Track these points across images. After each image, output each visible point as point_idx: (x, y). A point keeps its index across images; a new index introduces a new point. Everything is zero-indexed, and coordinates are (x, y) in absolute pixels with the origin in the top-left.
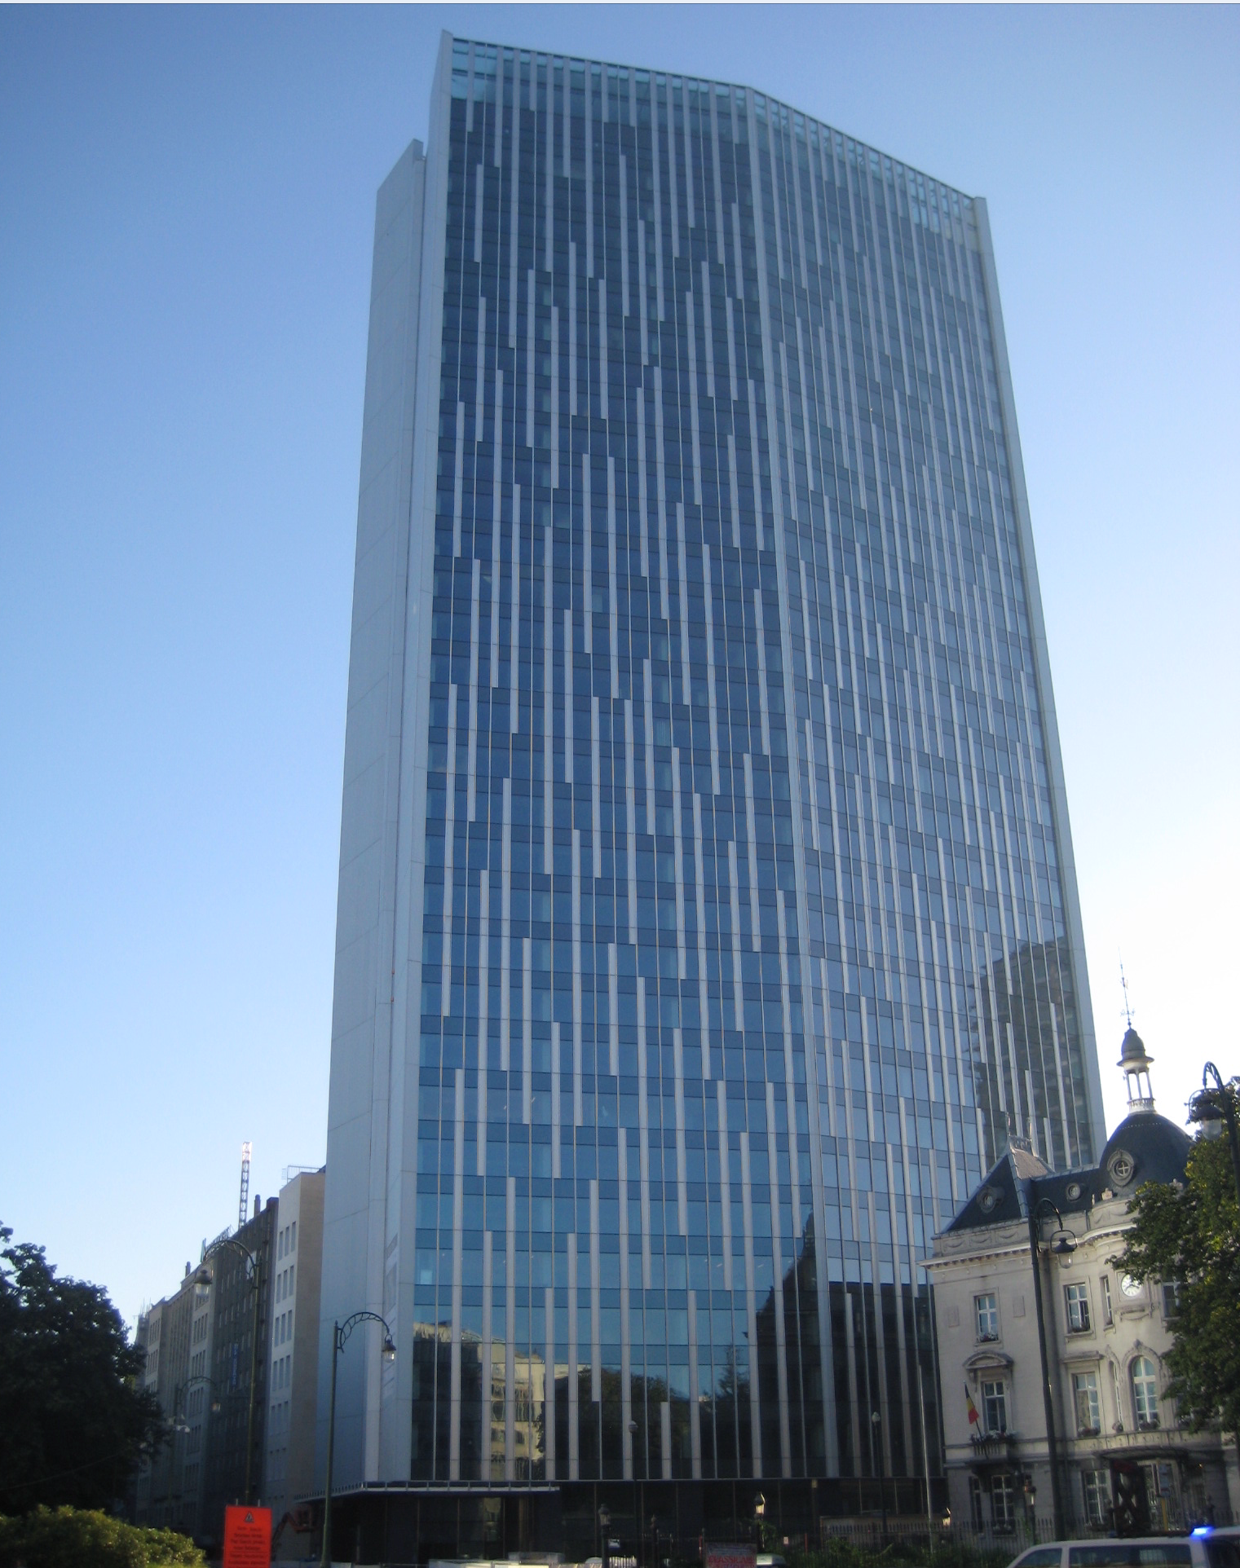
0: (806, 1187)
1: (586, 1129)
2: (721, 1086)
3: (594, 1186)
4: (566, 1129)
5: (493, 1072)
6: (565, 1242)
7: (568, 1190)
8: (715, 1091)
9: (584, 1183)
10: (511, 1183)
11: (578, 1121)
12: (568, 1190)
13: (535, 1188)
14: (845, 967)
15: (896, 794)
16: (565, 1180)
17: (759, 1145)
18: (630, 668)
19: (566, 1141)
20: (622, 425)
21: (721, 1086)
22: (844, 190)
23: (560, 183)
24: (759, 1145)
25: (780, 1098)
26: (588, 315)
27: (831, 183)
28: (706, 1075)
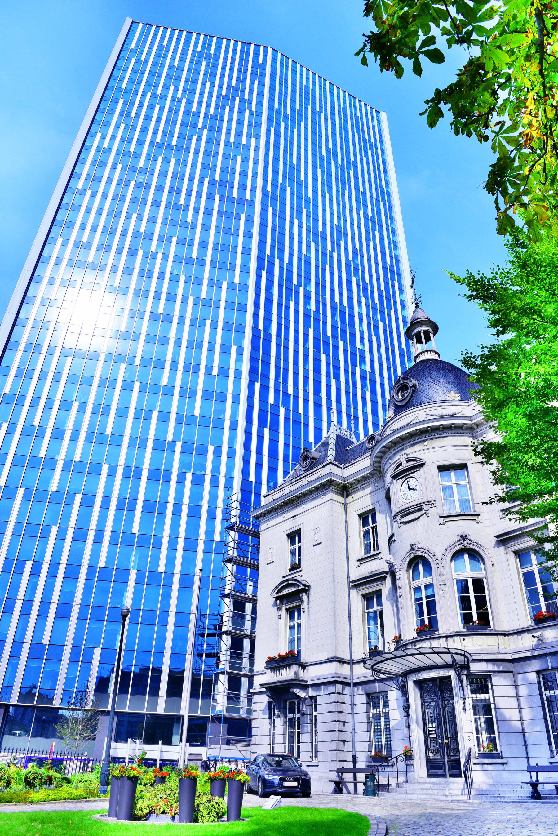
0: (312, 723)
1: (106, 570)
2: (179, 445)
3: (78, 498)
4: (92, 568)
5: (27, 426)
6: (49, 531)
7: (62, 499)
8: (174, 447)
9: (72, 495)
10: (21, 492)
11: (77, 458)
12: (62, 499)
13: (37, 495)
14: (291, 435)
15: (314, 319)
16: (59, 492)
17: (198, 481)
18: (165, 240)
19: (65, 469)
20: (182, 149)
21: (179, 445)
22: (314, 91)
23: (171, 67)
24: (198, 481)
25: (217, 454)
26: (174, 111)
27: (307, 87)
28: (170, 437)
